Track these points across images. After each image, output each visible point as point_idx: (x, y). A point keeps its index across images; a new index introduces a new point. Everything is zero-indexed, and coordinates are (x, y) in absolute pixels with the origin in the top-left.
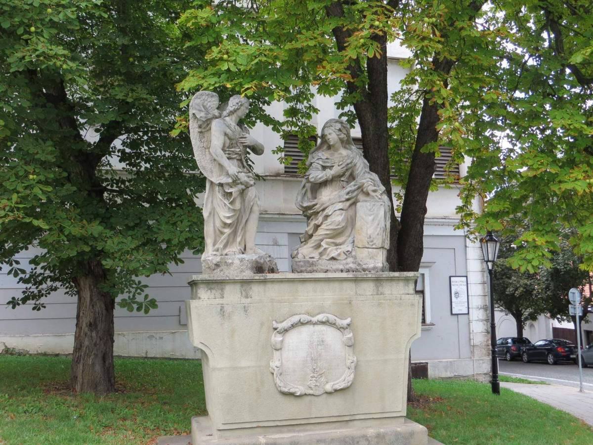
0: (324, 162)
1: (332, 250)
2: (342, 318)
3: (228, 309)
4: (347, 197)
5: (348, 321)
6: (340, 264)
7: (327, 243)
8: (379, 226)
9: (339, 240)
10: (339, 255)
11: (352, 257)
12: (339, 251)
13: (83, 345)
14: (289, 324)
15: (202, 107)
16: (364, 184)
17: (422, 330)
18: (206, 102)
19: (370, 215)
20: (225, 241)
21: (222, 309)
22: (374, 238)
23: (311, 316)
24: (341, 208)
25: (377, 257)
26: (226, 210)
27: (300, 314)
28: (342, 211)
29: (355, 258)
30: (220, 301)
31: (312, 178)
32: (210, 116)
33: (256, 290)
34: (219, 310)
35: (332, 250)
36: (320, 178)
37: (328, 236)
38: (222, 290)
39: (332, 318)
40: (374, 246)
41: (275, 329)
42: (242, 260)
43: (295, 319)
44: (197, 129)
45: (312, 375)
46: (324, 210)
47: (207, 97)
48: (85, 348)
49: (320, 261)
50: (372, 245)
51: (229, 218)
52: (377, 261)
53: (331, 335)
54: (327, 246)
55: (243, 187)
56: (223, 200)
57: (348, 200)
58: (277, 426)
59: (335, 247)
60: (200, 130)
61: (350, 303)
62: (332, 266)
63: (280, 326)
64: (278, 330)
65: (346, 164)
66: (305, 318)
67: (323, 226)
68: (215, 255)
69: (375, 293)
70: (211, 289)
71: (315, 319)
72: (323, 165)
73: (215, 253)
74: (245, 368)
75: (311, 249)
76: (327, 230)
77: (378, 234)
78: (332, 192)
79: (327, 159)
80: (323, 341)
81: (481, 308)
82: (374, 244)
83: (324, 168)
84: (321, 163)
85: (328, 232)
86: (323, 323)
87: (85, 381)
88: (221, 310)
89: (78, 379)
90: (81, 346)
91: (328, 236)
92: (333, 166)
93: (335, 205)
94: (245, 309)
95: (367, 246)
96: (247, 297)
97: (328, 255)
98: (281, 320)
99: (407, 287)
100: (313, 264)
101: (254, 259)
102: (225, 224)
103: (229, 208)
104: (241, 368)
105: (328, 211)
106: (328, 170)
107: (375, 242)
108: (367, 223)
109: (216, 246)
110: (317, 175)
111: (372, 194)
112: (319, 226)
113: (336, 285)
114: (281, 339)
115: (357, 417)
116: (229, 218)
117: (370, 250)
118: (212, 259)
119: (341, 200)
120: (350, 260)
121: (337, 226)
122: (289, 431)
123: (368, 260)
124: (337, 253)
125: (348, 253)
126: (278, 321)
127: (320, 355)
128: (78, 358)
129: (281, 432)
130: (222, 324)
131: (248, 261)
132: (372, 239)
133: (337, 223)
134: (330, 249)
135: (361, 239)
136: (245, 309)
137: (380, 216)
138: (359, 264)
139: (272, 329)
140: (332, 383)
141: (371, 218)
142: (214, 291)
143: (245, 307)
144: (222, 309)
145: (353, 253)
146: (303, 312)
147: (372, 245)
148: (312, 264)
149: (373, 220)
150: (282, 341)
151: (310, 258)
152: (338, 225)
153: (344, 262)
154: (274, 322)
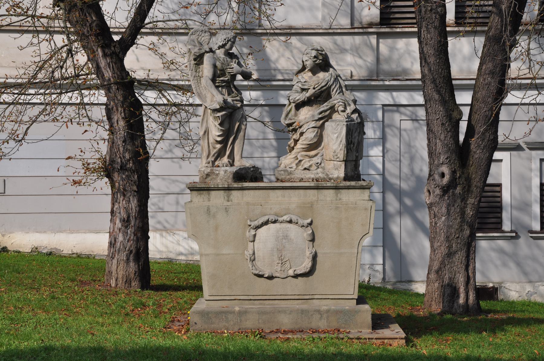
0: (303, 85)
1: (305, 162)
2: (304, 217)
3: (213, 210)
4: (320, 116)
5: (309, 221)
6: (312, 174)
7: (302, 156)
8: (342, 143)
9: (313, 153)
10: (311, 166)
11: (322, 168)
12: (311, 162)
13: (117, 240)
14: (260, 223)
15: (196, 42)
16: (335, 105)
17: (374, 228)
18: (200, 37)
19: (336, 133)
20: (216, 155)
21: (208, 209)
22: (338, 153)
23: (277, 216)
24: (313, 126)
25: (340, 168)
26: (217, 130)
27: (270, 215)
28: (315, 129)
29: (323, 168)
30: (207, 203)
31: (291, 99)
32: (203, 51)
33: (235, 193)
34: (206, 210)
35: (305, 162)
36: (298, 100)
37: (304, 150)
38: (209, 194)
39: (294, 218)
40: (338, 160)
41: (250, 226)
42: (226, 171)
43: (265, 219)
44: (193, 62)
45: (277, 262)
46: (300, 127)
47: (201, 33)
48: (119, 244)
49: (297, 170)
50: (337, 158)
51: (219, 136)
52: (340, 172)
53: (293, 231)
54: (302, 159)
55: (230, 110)
56: (214, 121)
57: (320, 119)
58: (251, 300)
59: (309, 159)
60: (195, 62)
61: (312, 207)
62: (305, 175)
63: (254, 224)
64: (251, 226)
65: (320, 86)
66: (272, 218)
67: (300, 142)
68: (207, 167)
69: (334, 199)
70: (200, 194)
71: (280, 219)
72: (302, 87)
73: (207, 165)
74: (226, 254)
75: (293, 160)
76: (302, 144)
77: (341, 150)
78: (309, 111)
79: (305, 82)
80: (287, 236)
81: (343, 161)
82: (338, 158)
83: (303, 90)
84: (300, 85)
85: (304, 147)
86: (290, 222)
87: (120, 276)
88: (208, 210)
89: (113, 274)
90: (115, 241)
91: (304, 150)
92: (309, 89)
93: (308, 124)
94: (226, 210)
95: (333, 159)
96: (228, 201)
97: (302, 166)
98: (255, 219)
99: (362, 195)
100: (291, 173)
101: (234, 171)
102: (217, 141)
103: (218, 129)
104: (223, 254)
105: (304, 129)
106: (304, 93)
107: (339, 156)
108: (333, 139)
109: (209, 159)
110: (295, 97)
111: (340, 113)
112: (298, 140)
113: (302, 192)
114: (254, 233)
115: (316, 297)
116: (219, 136)
117: (335, 162)
118: (204, 171)
119: (314, 119)
120: (320, 170)
121: (310, 141)
122: (261, 304)
123: (334, 171)
124: (309, 164)
125: (318, 165)
126: (252, 219)
127: (284, 247)
128: (113, 254)
129: (254, 304)
130: (208, 221)
131: (230, 172)
132: (336, 153)
133: (310, 139)
134: (304, 161)
135: (328, 154)
136: (226, 210)
137: (342, 134)
138: (327, 175)
139: (248, 226)
140: (294, 269)
141: (336, 135)
142: (203, 196)
143: (226, 208)
144: (208, 209)
145: (323, 165)
146: (272, 213)
147: (337, 158)
148: (290, 173)
149: (337, 137)
150: (255, 236)
151: (290, 168)
152: (310, 141)
153: (315, 172)
154: (248, 221)
